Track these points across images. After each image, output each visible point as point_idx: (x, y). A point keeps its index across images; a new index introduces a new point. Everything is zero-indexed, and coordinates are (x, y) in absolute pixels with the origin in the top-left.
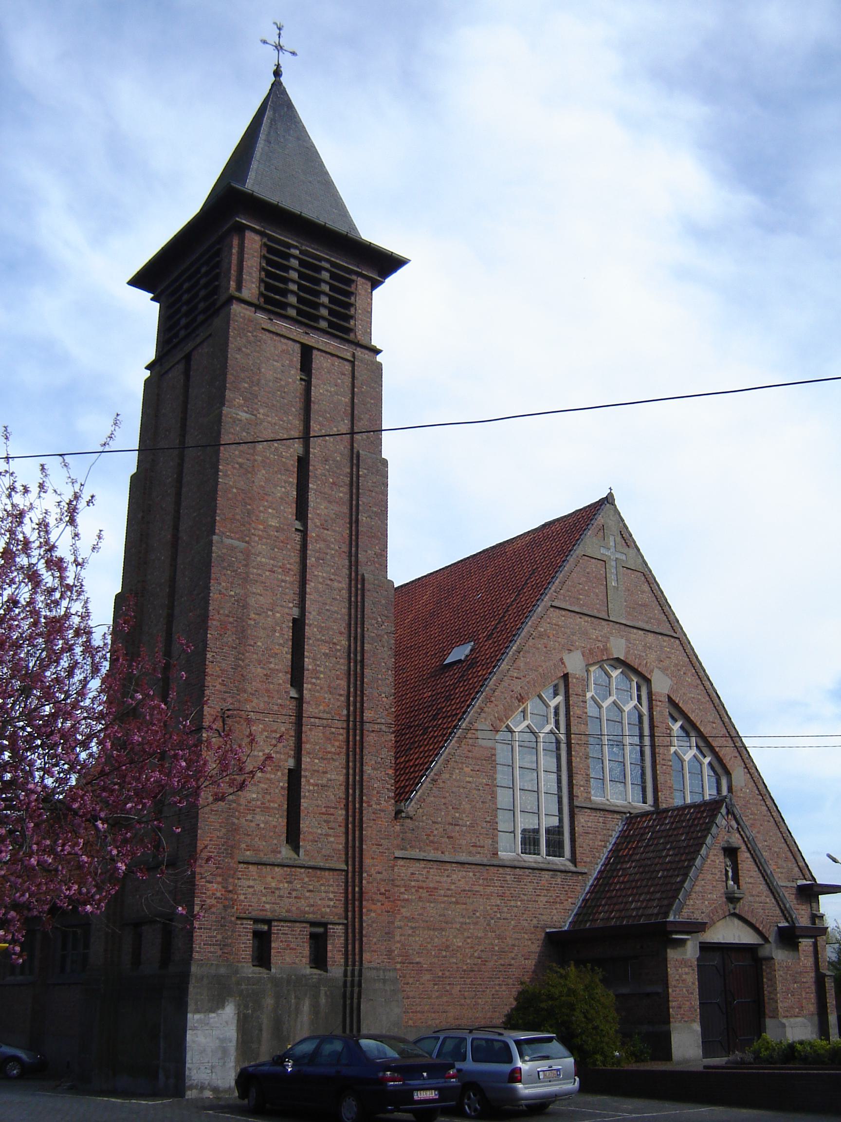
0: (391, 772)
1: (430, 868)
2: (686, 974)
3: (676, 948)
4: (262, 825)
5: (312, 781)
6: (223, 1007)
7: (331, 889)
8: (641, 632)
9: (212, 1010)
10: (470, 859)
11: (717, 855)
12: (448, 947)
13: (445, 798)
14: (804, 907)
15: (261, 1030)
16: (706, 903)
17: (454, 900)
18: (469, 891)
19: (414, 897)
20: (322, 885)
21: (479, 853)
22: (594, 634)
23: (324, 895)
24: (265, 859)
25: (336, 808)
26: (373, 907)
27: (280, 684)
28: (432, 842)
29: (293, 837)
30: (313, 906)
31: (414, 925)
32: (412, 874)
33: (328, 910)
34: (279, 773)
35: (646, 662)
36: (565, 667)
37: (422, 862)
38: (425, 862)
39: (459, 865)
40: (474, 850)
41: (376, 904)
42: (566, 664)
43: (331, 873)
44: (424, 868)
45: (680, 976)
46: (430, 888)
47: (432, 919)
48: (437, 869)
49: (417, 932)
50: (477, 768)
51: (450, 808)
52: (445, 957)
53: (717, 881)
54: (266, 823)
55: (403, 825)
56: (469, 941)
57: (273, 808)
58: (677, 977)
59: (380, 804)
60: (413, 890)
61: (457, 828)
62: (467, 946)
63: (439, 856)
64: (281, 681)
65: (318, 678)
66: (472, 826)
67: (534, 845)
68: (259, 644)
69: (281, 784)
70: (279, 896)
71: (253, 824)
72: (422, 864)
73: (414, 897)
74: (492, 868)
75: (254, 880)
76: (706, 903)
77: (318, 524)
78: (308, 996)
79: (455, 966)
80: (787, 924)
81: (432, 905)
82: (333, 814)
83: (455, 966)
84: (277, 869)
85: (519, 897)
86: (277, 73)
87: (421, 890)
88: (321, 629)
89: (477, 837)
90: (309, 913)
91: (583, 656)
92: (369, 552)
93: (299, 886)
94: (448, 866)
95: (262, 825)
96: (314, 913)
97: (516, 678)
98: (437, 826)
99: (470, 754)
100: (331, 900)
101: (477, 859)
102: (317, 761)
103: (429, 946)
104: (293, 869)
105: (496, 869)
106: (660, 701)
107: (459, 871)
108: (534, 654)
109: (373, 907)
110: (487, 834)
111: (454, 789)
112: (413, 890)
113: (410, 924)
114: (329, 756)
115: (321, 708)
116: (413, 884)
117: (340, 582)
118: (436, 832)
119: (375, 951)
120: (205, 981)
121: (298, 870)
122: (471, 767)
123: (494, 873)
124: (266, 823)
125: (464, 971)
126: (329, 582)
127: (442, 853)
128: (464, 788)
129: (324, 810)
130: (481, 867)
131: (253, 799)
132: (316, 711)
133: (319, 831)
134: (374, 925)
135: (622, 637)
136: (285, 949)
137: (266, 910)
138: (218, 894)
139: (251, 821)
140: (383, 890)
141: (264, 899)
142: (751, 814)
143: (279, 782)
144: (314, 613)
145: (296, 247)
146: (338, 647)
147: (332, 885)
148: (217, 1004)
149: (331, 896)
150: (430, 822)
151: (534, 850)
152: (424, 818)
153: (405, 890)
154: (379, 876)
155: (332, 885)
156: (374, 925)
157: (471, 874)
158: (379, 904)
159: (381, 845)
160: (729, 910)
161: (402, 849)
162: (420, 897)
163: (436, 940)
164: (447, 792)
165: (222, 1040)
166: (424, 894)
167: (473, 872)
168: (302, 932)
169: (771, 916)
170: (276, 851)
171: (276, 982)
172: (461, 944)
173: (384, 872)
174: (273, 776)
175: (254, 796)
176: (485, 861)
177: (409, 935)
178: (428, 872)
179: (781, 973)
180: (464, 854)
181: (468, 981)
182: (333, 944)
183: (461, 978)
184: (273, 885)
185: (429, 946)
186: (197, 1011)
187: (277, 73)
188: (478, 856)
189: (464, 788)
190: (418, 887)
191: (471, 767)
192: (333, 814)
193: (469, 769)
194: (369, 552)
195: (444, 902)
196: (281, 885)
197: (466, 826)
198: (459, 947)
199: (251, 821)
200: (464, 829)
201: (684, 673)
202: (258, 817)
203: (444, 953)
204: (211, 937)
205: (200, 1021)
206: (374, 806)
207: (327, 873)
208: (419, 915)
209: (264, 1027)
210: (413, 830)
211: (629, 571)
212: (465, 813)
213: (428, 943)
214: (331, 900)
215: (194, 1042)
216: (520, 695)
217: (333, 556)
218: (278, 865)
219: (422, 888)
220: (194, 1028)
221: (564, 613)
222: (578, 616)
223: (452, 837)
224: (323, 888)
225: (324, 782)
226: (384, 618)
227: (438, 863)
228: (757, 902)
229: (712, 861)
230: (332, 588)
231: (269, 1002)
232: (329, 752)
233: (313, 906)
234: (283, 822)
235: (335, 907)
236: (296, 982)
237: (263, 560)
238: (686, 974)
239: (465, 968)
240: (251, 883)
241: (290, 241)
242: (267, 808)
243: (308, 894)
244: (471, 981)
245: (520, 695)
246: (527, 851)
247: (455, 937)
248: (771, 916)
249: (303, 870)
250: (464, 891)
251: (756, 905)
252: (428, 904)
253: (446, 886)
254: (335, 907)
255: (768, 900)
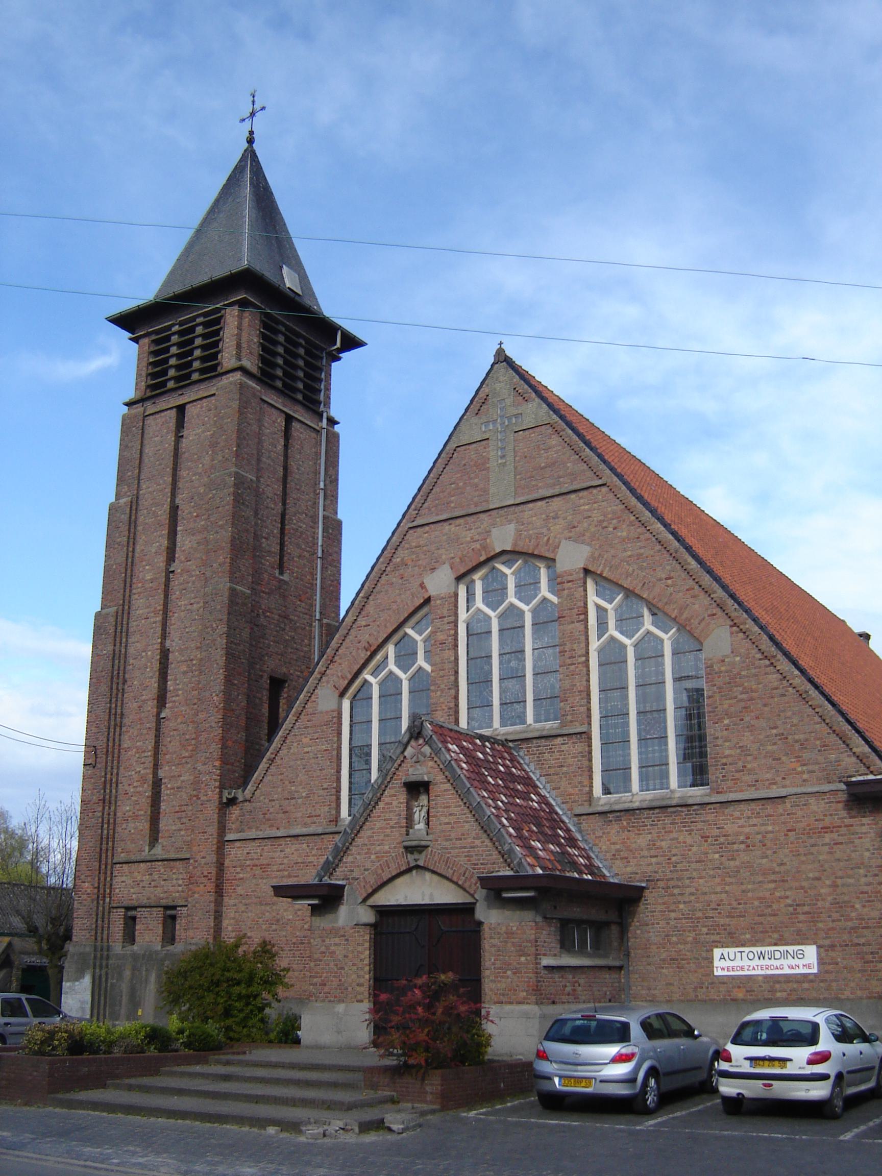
0: (217, 763)
1: (265, 846)
2: (336, 944)
3: (324, 916)
4: (132, 831)
5: (169, 786)
6: (83, 977)
7: (181, 876)
8: (539, 504)
9: (77, 980)
10: (305, 831)
11: (395, 795)
12: (278, 921)
13: (282, 774)
14: (865, 820)
15: (121, 997)
16: (373, 857)
17: (286, 873)
18: (302, 863)
19: (249, 875)
20: (174, 873)
21: (315, 823)
22: (467, 536)
23: (175, 881)
24: (133, 858)
25: (187, 805)
26: (196, 889)
27: (149, 711)
28: (269, 820)
29: (154, 838)
30: (166, 892)
31: (247, 902)
32: (248, 853)
33: (177, 895)
34: (146, 786)
35: (549, 539)
36: (427, 591)
37: (256, 841)
38: (260, 841)
39: (293, 839)
40: (308, 820)
41: (199, 886)
42: (427, 587)
43: (181, 862)
44: (259, 846)
45: (327, 948)
46: (263, 865)
47: (264, 894)
48: (271, 845)
49: (250, 908)
50: (316, 735)
51: (287, 783)
52: (276, 930)
53: (392, 827)
54: (135, 828)
55: (241, 809)
56: (299, 913)
57: (141, 815)
58: (323, 949)
59: (206, 795)
60: (248, 869)
61: (293, 801)
62: (298, 918)
63: (274, 833)
64: (150, 708)
65: (177, 695)
66: (308, 797)
67: (662, 778)
68: (135, 683)
69: (147, 794)
70: (143, 887)
71: (127, 831)
72: (257, 843)
73: (249, 875)
74: (326, 836)
75: (126, 876)
76: (373, 857)
77: (183, 559)
78: (155, 968)
79: (284, 939)
80: (511, 873)
81: (264, 881)
82: (184, 811)
83: (284, 939)
84: (142, 865)
85: (654, 845)
86: (251, 141)
87: (254, 868)
88: (181, 651)
89: (313, 806)
90: (163, 899)
91: (452, 568)
92: (215, 565)
93: (156, 877)
94: (282, 841)
95: (132, 831)
96: (167, 898)
97: (365, 626)
98: (273, 803)
99: (309, 724)
100: (180, 886)
101: (312, 829)
102: (173, 768)
103: (261, 921)
104: (153, 863)
105: (331, 836)
106: (569, 582)
107: (292, 844)
108: (387, 591)
109: (196, 889)
110: (323, 802)
111: (292, 763)
112: (248, 869)
113: (243, 901)
114: (184, 760)
115: (179, 720)
116: (248, 863)
117: (198, 603)
118: (271, 810)
119: (197, 929)
120: (76, 957)
121: (157, 863)
122: (309, 737)
123: (329, 841)
124: (135, 828)
125: (294, 943)
126: (189, 607)
127: (278, 829)
128: (302, 759)
129: (177, 809)
130: (316, 837)
131: (127, 811)
132: (175, 724)
133: (173, 828)
134: (197, 905)
135: (510, 522)
136: (145, 930)
137: (133, 900)
138: (89, 891)
139: (125, 829)
140: (206, 873)
141: (132, 890)
142: (742, 693)
143: (146, 792)
144: (176, 640)
145: (173, 325)
146: (194, 662)
147: (181, 873)
148: (79, 976)
149: (180, 882)
150: (267, 801)
151: (662, 784)
152: (262, 798)
153: (242, 870)
154: (203, 861)
155: (181, 873)
156: (197, 905)
157: (304, 846)
158: (202, 886)
159: (206, 832)
160: (408, 863)
161: (240, 832)
162: (255, 875)
163: (267, 914)
164: (285, 767)
165: (83, 1002)
166: (258, 871)
167: (308, 843)
168: (158, 913)
169: (482, 864)
170: (141, 851)
171: (135, 957)
172: (291, 917)
173: (207, 856)
174: (141, 789)
175: (128, 808)
176: (320, 830)
177: (243, 912)
178: (263, 849)
179: (495, 941)
180: (299, 826)
181: (297, 953)
182: (180, 923)
183: (290, 951)
184: (139, 878)
185: (260, 920)
186: (68, 981)
187: (251, 141)
188: (314, 826)
189: (302, 759)
190: (253, 866)
191: (309, 737)
192: (184, 811)
193: (308, 739)
194: (215, 565)
195: (276, 877)
196: (144, 878)
197: (302, 798)
198: (289, 920)
199: (125, 829)
200: (300, 801)
201: (615, 529)
202: (129, 824)
203: (274, 927)
204: (84, 924)
205: (70, 988)
206: (202, 798)
207: (178, 863)
208: (253, 891)
209: (124, 994)
210: (251, 812)
211: (527, 432)
212: (301, 785)
213: (260, 918)
214: (180, 886)
215: (66, 1003)
216: (368, 643)
217: (194, 582)
218: (143, 862)
219: (256, 866)
220: (67, 993)
221: (427, 528)
222: (445, 524)
223: (287, 812)
224: (174, 876)
225: (179, 784)
226: (218, 622)
227: (272, 840)
228: (457, 848)
229: (387, 804)
230: (191, 611)
231: (127, 973)
232: (184, 757)
233: (166, 892)
234: (147, 826)
235: (183, 891)
236: (149, 957)
237: (141, 612)
238: (336, 944)
239: (294, 940)
240: (124, 879)
241: (166, 324)
242: (137, 816)
243: (163, 883)
244: (301, 954)
245: (368, 643)
246: (657, 787)
247: (285, 910)
248: (482, 864)
249: (160, 863)
250: (297, 863)
251: (455, 852)
252: (260, 881)
253: (279, 861)
254: (183, 891)
255: (478, 842)
